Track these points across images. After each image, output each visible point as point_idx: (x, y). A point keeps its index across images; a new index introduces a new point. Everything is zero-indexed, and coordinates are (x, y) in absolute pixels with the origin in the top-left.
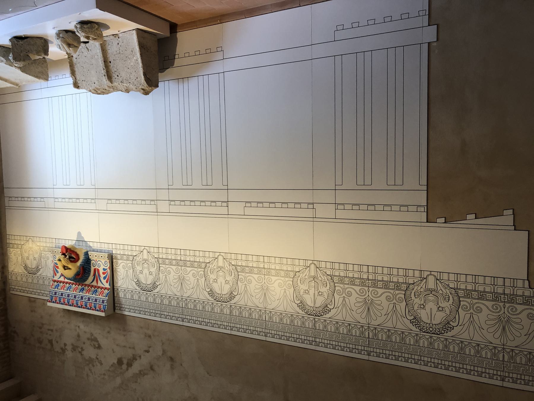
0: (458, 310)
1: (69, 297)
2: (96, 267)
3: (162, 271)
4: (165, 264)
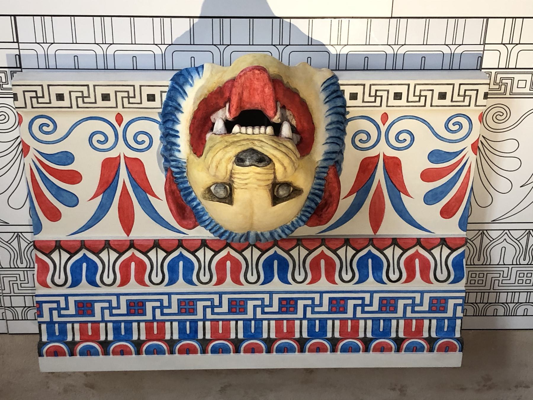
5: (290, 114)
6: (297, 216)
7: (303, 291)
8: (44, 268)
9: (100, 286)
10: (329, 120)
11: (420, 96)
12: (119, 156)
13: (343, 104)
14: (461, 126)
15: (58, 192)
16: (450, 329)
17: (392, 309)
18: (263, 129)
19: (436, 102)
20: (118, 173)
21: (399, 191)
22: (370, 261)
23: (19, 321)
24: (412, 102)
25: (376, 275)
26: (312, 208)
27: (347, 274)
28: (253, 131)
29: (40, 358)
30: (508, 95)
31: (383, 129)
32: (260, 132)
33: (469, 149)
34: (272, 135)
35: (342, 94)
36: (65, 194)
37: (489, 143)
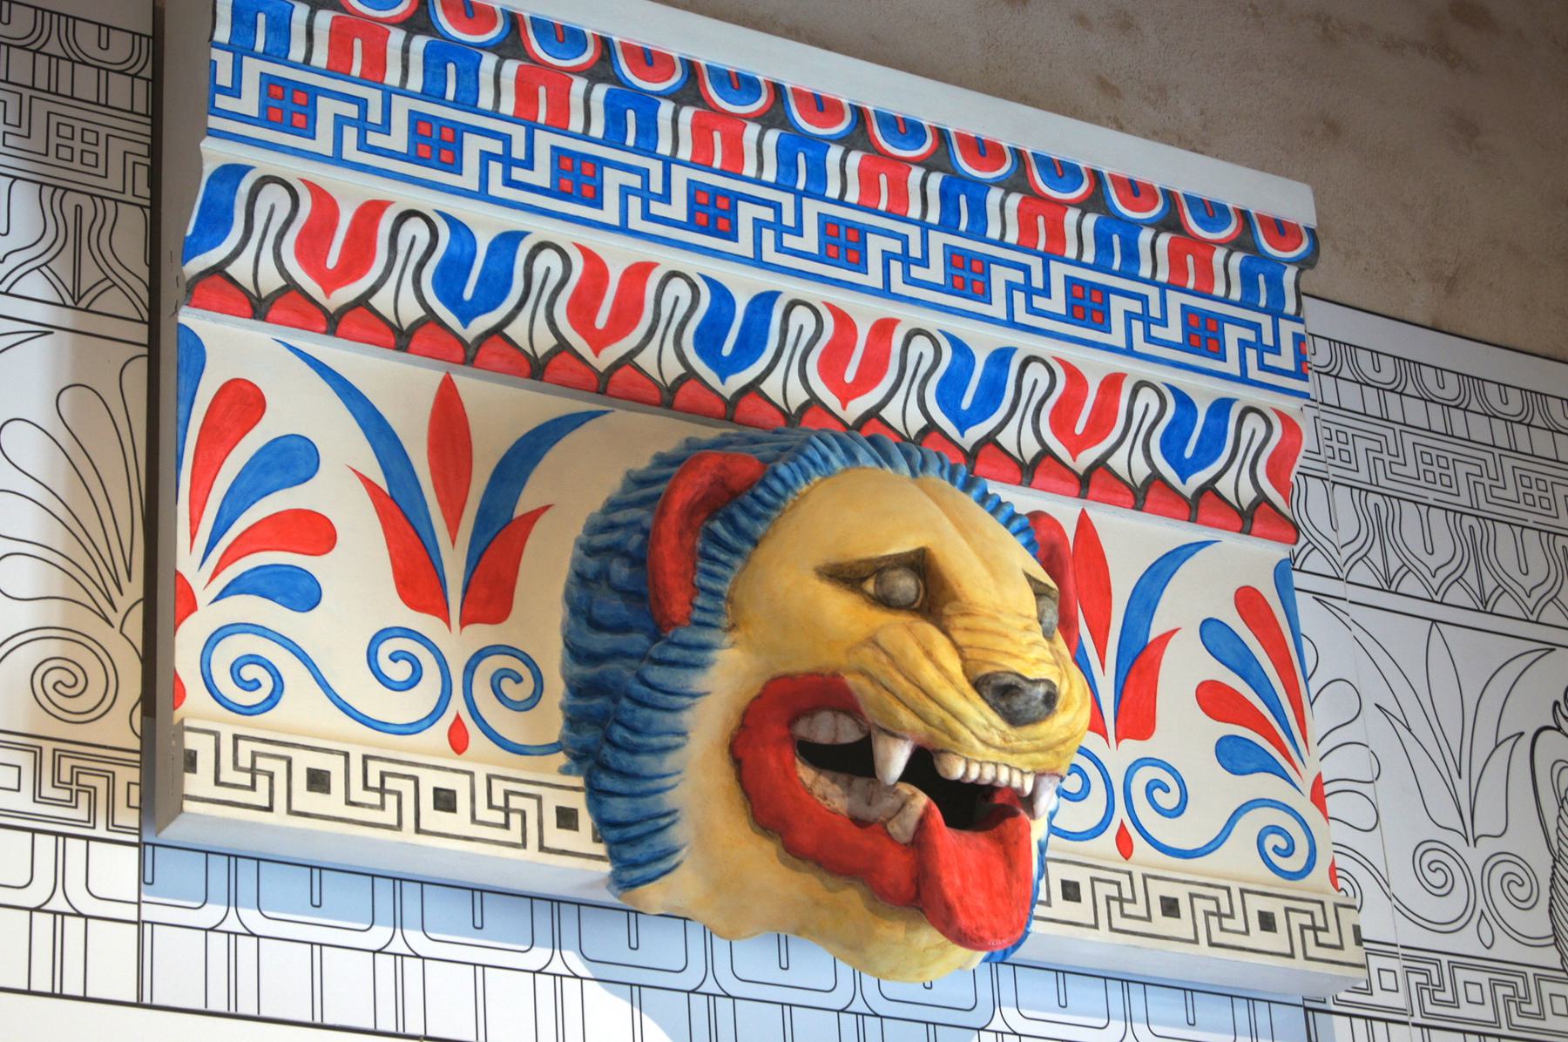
0: (1554, 867)
1: (954, 258)
2: (458, 642)
3: (1522, 893)
4: (1502, 971)
5: (825, 798)
6: (797, 498)
7: (672, 246)
8: (1279, 469)
9: (824, 306)
10: (670, 762)
11: (382, 790)
12: (1118, 740)
13: (599, 803)
14: (235, 670)
15: (1244, 665)
16: (248, 17)
17: (424, 128)
18: (974, 774)
19: (334, 765)
20: (1118, 693)
21: (392, 498)
22: (468, 294)
23: (100, 21)
24: (405, 777)
25: (468, 249)
26: (746, 510)
27: (548, 269)
28: (997, 773)
29: (1313, 224)
30: (48, 747)
31: (457, 705)
32: (981, 768)
33: (203, 596)
34: (942, 751)
35: (600, 830)
36: (1230, 658)
37: (88, 597)
